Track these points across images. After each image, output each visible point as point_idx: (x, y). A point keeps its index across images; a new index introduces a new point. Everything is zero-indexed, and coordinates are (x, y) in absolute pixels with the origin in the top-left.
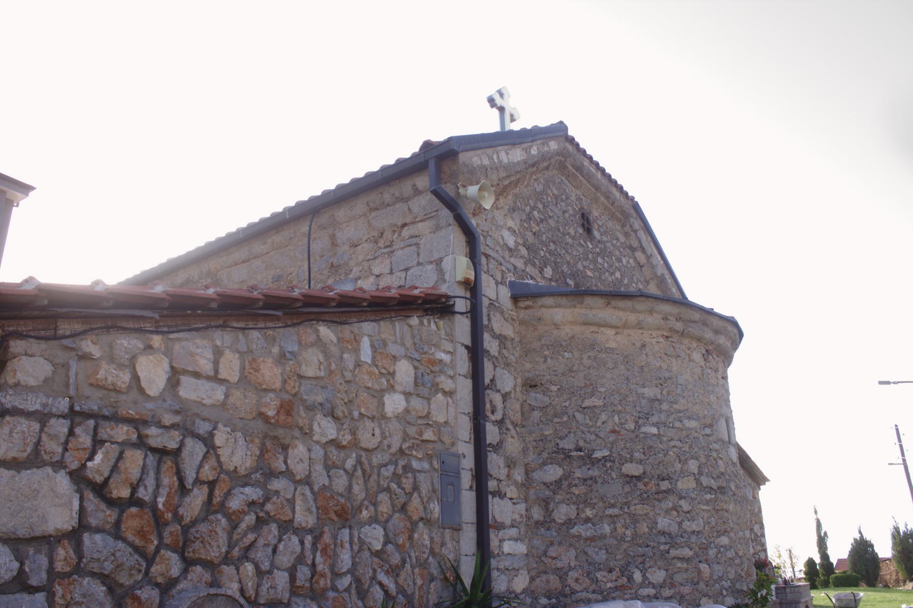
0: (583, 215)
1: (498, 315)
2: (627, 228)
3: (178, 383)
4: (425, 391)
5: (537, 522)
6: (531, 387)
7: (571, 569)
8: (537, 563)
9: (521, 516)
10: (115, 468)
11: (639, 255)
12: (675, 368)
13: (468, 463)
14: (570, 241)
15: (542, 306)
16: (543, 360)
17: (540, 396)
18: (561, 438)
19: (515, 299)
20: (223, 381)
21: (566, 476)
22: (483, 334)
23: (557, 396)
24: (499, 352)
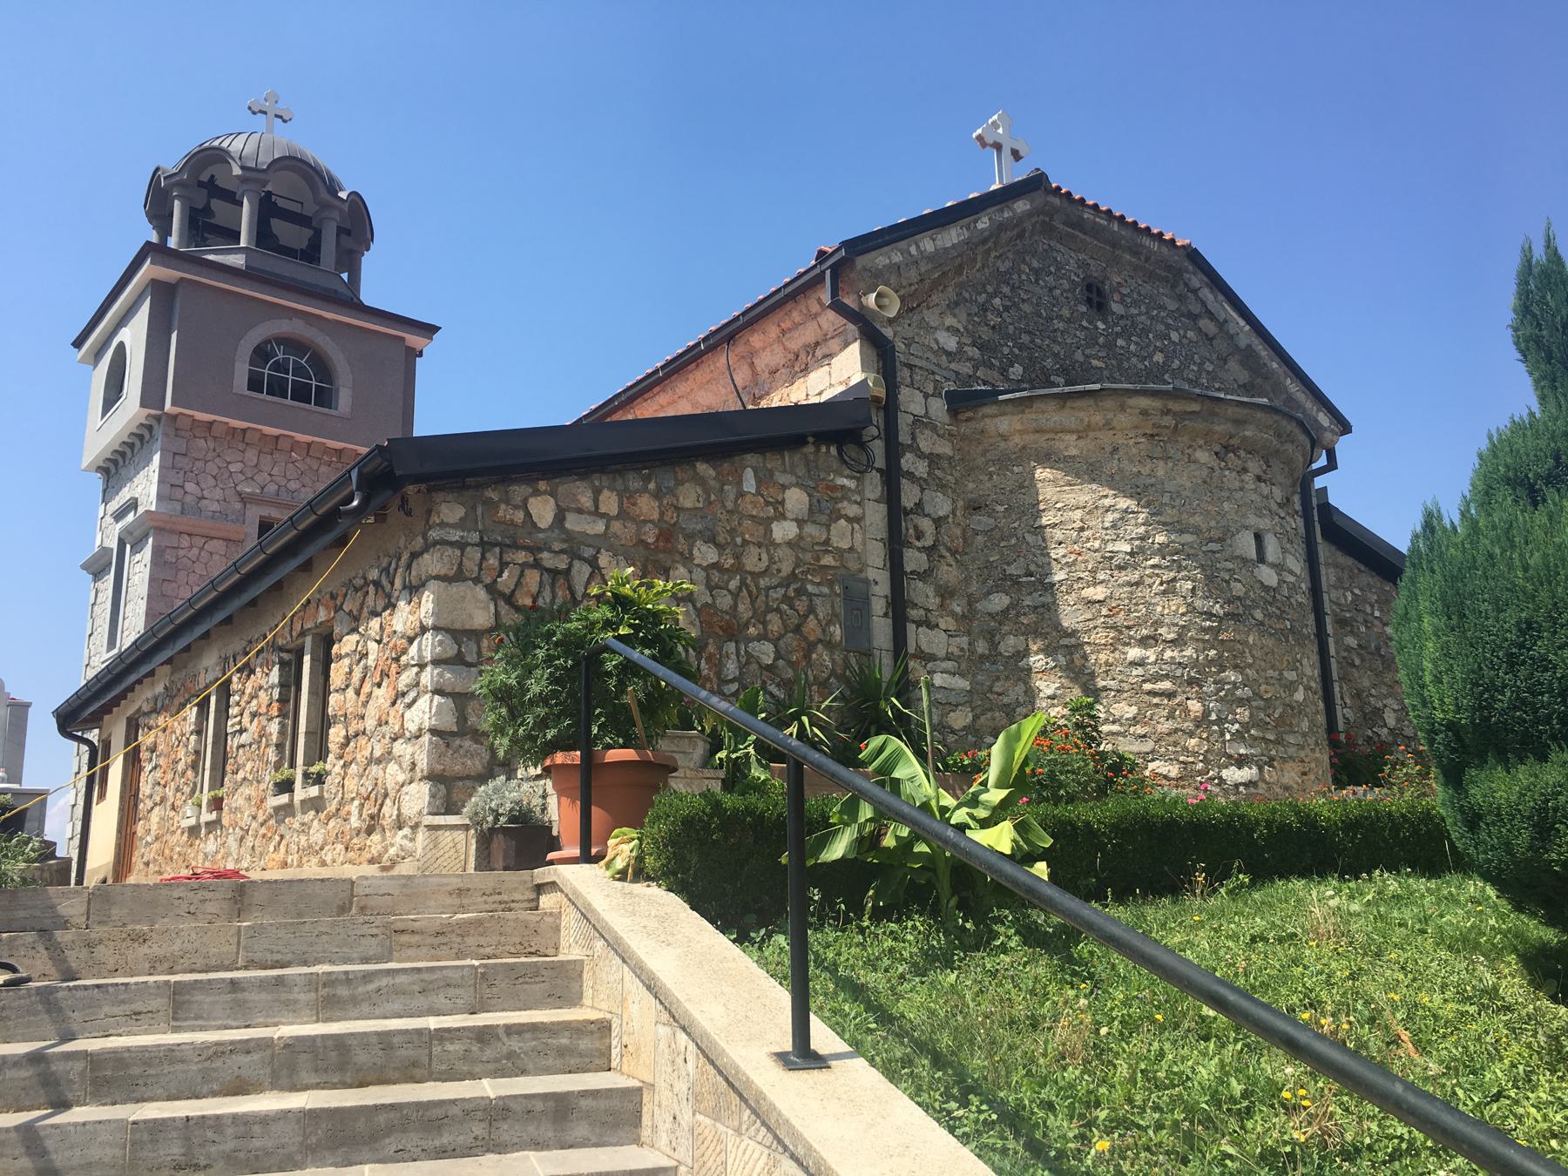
0: (1089, 287)
2: (1181, 288)
3: (564, 518)
4: (824, 518)
5: (982, 656)
7: (1019, 704)
10: (518, 584)
11: (1205, 323)
13: (882, 589)
14: (1061, 325)
15: (984, 416)
17: (984, 519)
18: (1009, 564)
19: (954, 412)
20: (603, 516)
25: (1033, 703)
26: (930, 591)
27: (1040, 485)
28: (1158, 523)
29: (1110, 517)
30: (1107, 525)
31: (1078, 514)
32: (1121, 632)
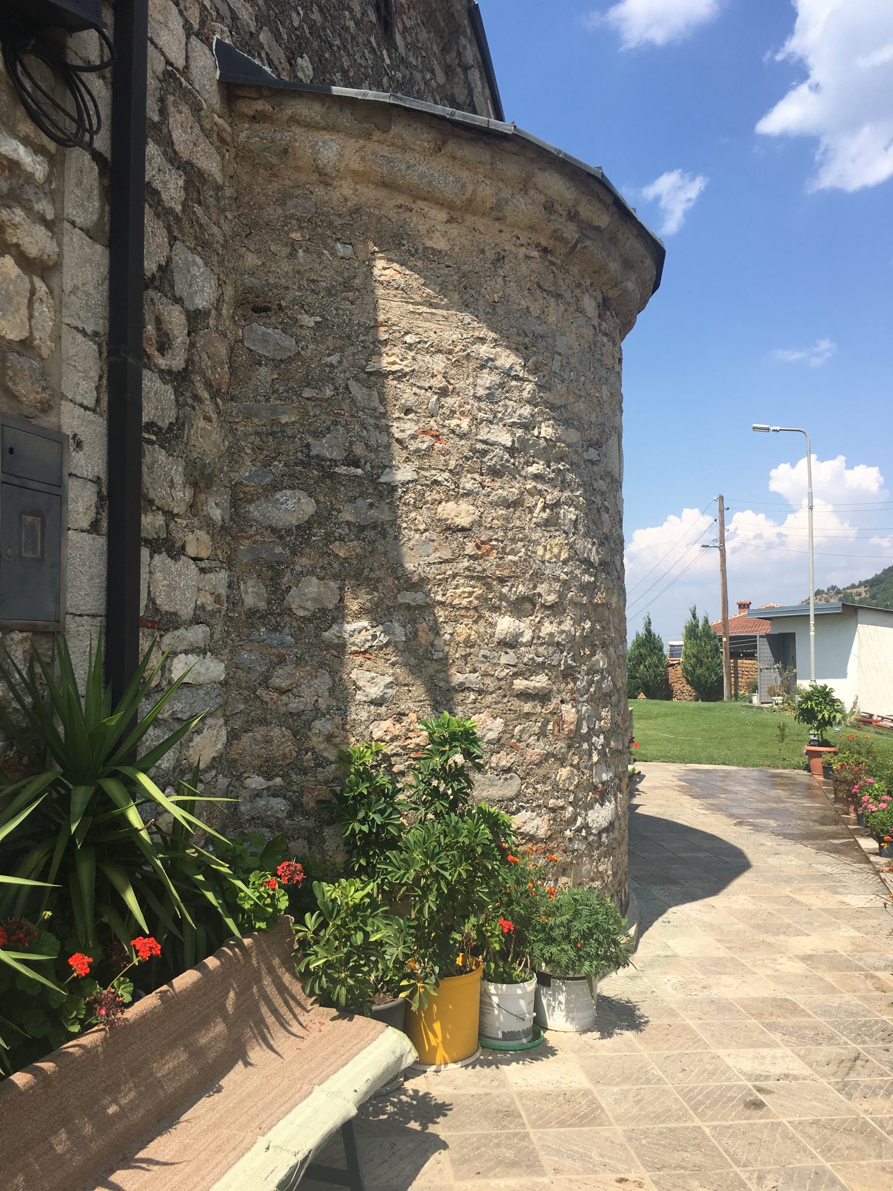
1: (185, 109)
2: (451, 57)
5: (252, 613)
6: (256, 310)
7: (318, 714)
8: (246, 701)
9: (218, 599)
12: (552, 319)
13: (89, 462)
15: (293, 120)
16: (286, 251)
17: (276, 334)
18: (317, 435)
21: (321, 518)
22: (144, 144)
23: (314, 340)
24: (184, 205)
25: (343, 711)
26: (177, 471)
27: (380, 292)
28: (546, 402)
29: (487, 379)
30: (481, 392)
31: (439, 363)
32: (489, 587)
